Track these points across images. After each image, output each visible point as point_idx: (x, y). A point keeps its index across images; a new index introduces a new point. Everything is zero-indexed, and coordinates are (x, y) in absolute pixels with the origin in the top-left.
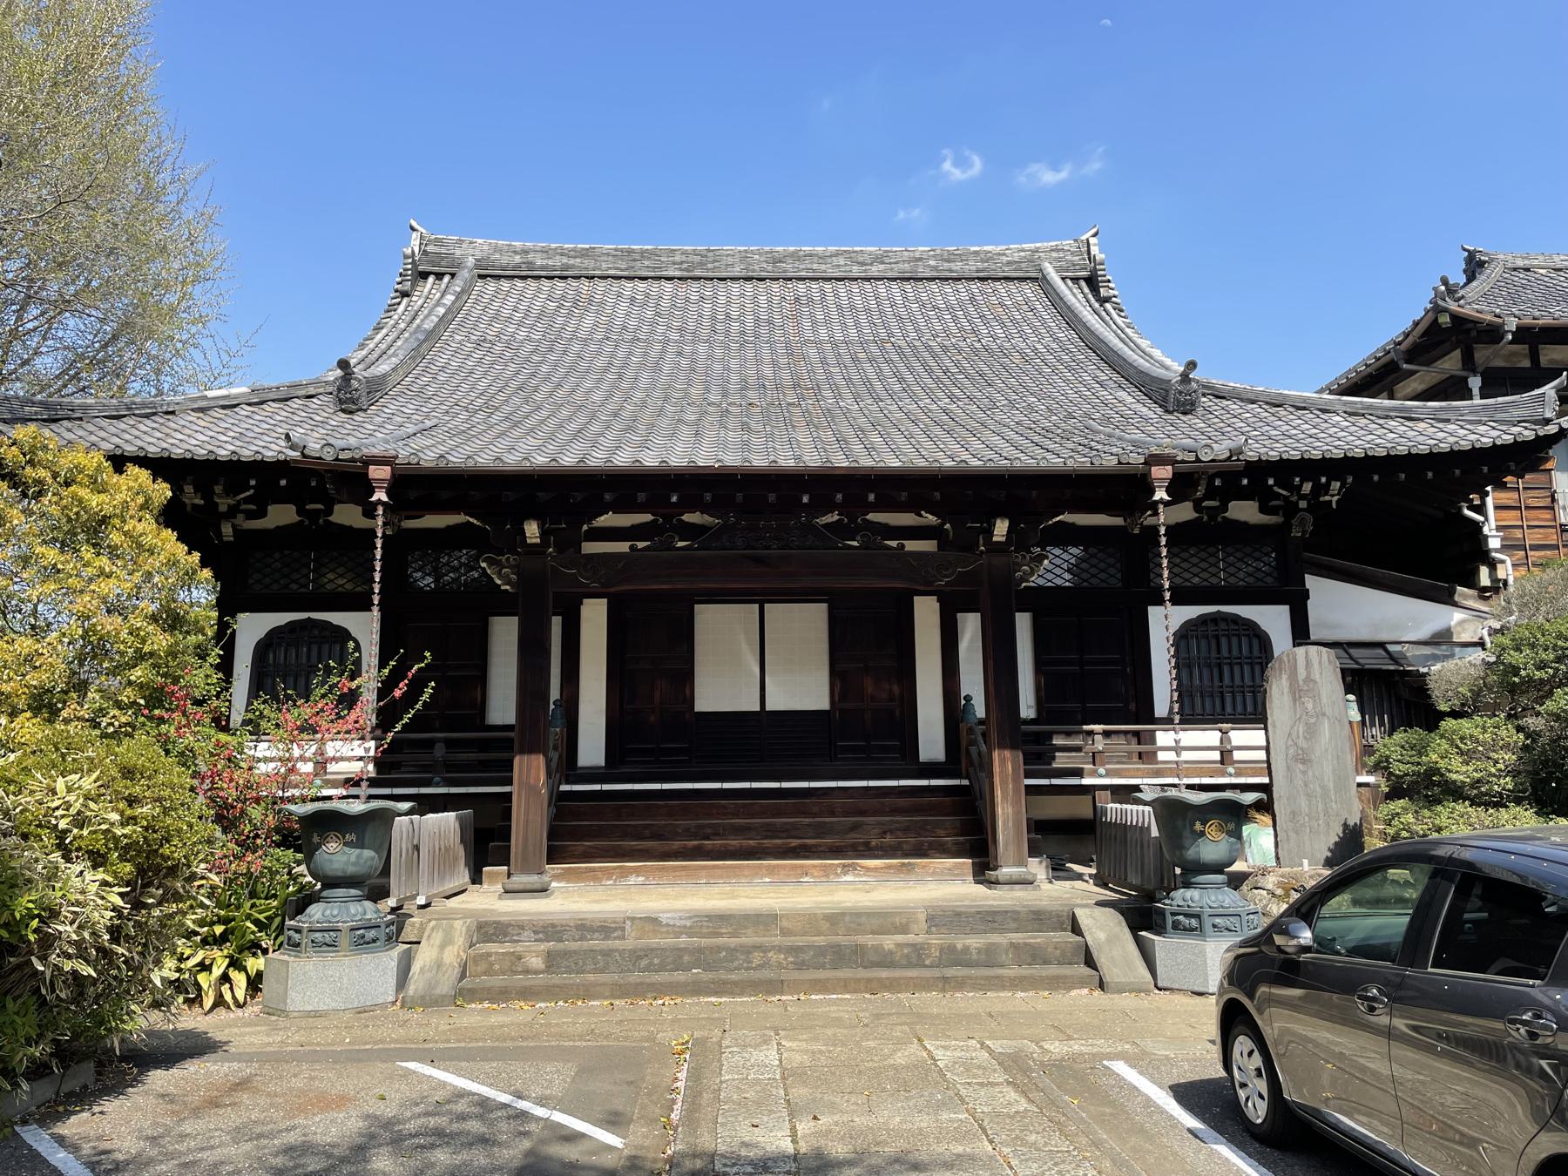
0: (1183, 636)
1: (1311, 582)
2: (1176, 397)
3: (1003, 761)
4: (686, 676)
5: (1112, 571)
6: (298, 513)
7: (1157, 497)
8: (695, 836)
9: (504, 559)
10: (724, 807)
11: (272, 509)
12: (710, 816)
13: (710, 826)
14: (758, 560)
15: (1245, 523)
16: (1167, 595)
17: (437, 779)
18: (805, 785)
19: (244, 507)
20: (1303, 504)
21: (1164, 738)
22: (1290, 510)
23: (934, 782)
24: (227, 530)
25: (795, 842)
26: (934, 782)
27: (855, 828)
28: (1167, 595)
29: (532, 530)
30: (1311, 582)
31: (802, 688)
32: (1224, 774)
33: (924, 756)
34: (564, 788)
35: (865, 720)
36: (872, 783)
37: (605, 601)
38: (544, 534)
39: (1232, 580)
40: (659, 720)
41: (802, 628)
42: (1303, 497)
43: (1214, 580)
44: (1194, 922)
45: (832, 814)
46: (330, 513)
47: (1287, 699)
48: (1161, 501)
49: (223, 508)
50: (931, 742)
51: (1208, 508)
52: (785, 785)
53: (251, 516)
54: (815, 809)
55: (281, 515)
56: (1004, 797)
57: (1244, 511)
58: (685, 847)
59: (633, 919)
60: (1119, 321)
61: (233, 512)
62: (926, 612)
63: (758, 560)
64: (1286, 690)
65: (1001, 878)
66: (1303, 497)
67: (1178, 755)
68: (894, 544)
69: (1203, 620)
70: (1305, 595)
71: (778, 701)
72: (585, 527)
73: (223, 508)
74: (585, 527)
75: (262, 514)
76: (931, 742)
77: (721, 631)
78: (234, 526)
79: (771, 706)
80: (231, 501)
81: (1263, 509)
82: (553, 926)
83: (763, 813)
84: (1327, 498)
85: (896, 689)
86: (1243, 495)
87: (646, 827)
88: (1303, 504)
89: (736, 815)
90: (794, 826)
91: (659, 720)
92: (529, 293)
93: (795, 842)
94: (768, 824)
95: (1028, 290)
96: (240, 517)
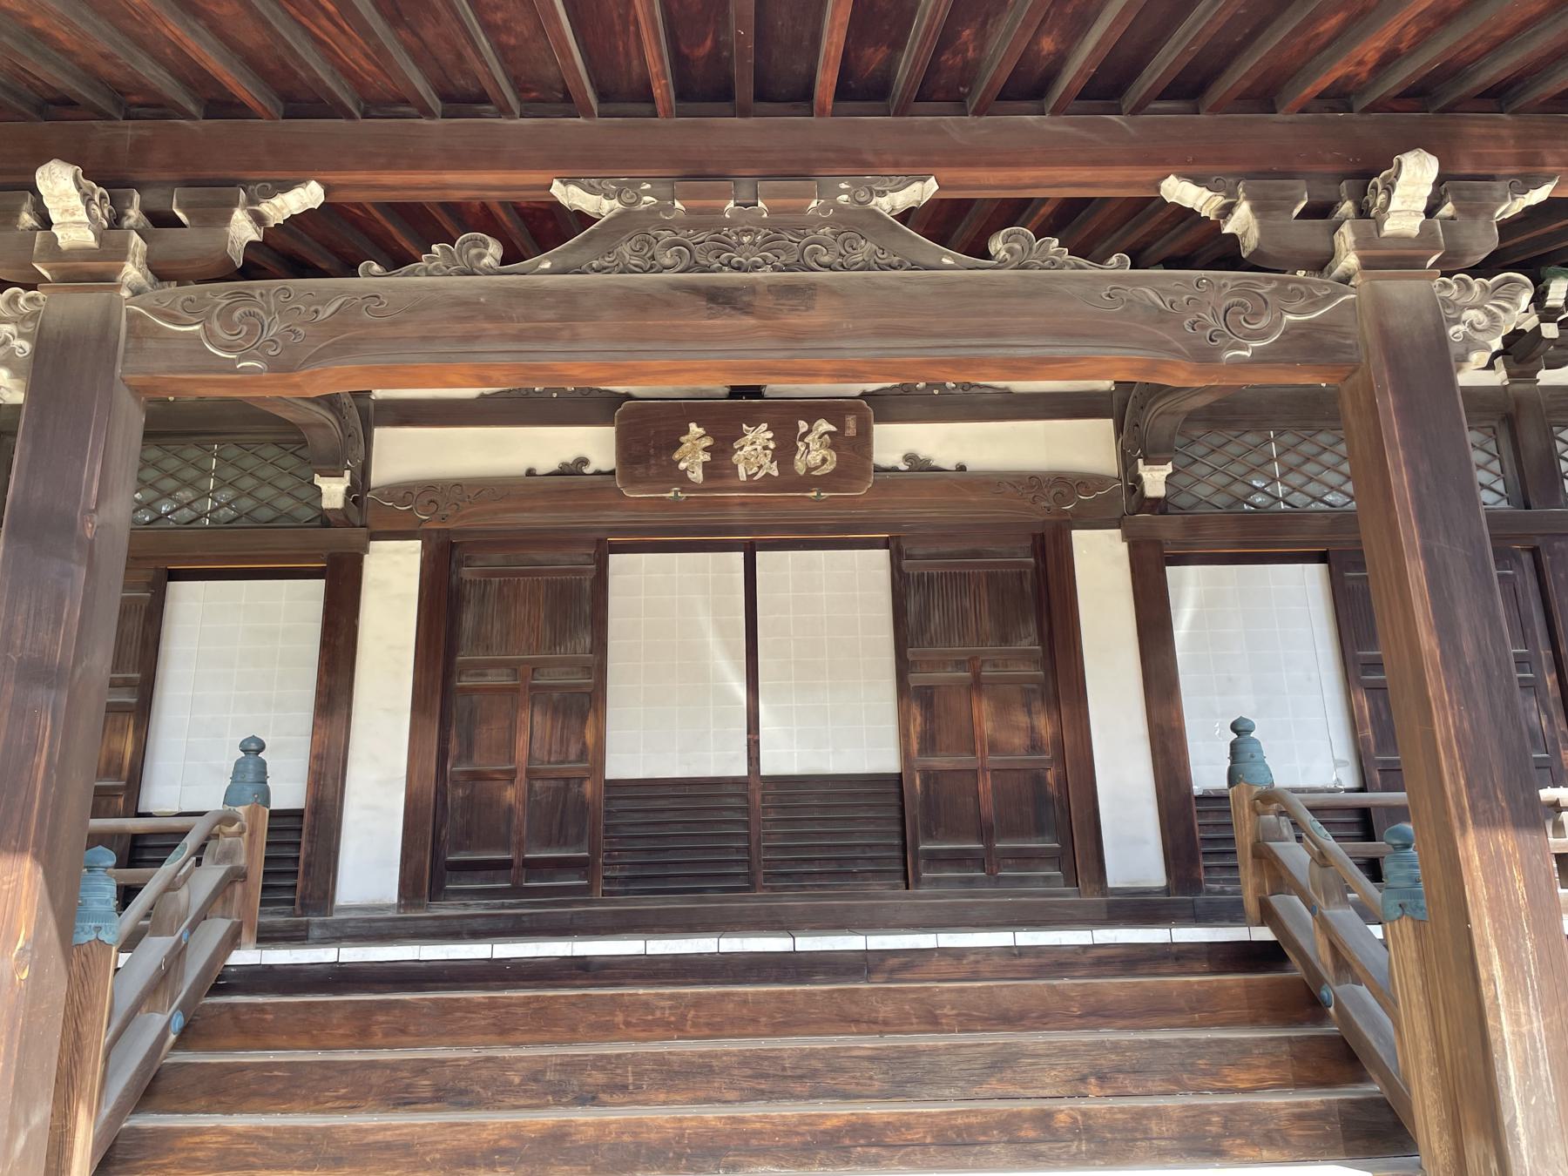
3: (1494, 867)
4: (585, 702)
8: (558, 1094)
10: (646, 1005)
12: (605, 1030)
13: (601, 1063)
14: (719, 298)
25: (838, 1112)
27: (1001, 1063)
31: (837, 720)
33: (1116, 877)
36: (1026, 938)
37: (417, 544)
41: (838, 598)
45: (932, 1022)
50: (1133, 849)
54: (886, 1010)
56: (1513, 965)
58: (517, 1133)
63: (719, 298)
76: (1133, 849)
77: (664, 604)
79: (766, 770)
83: (747, 1022)
85: (1045, 726)
87: (422, 1068)
89: (676, 1028)
90: (834, 1063)
93: (838, 1112)
94: (759, 1057)
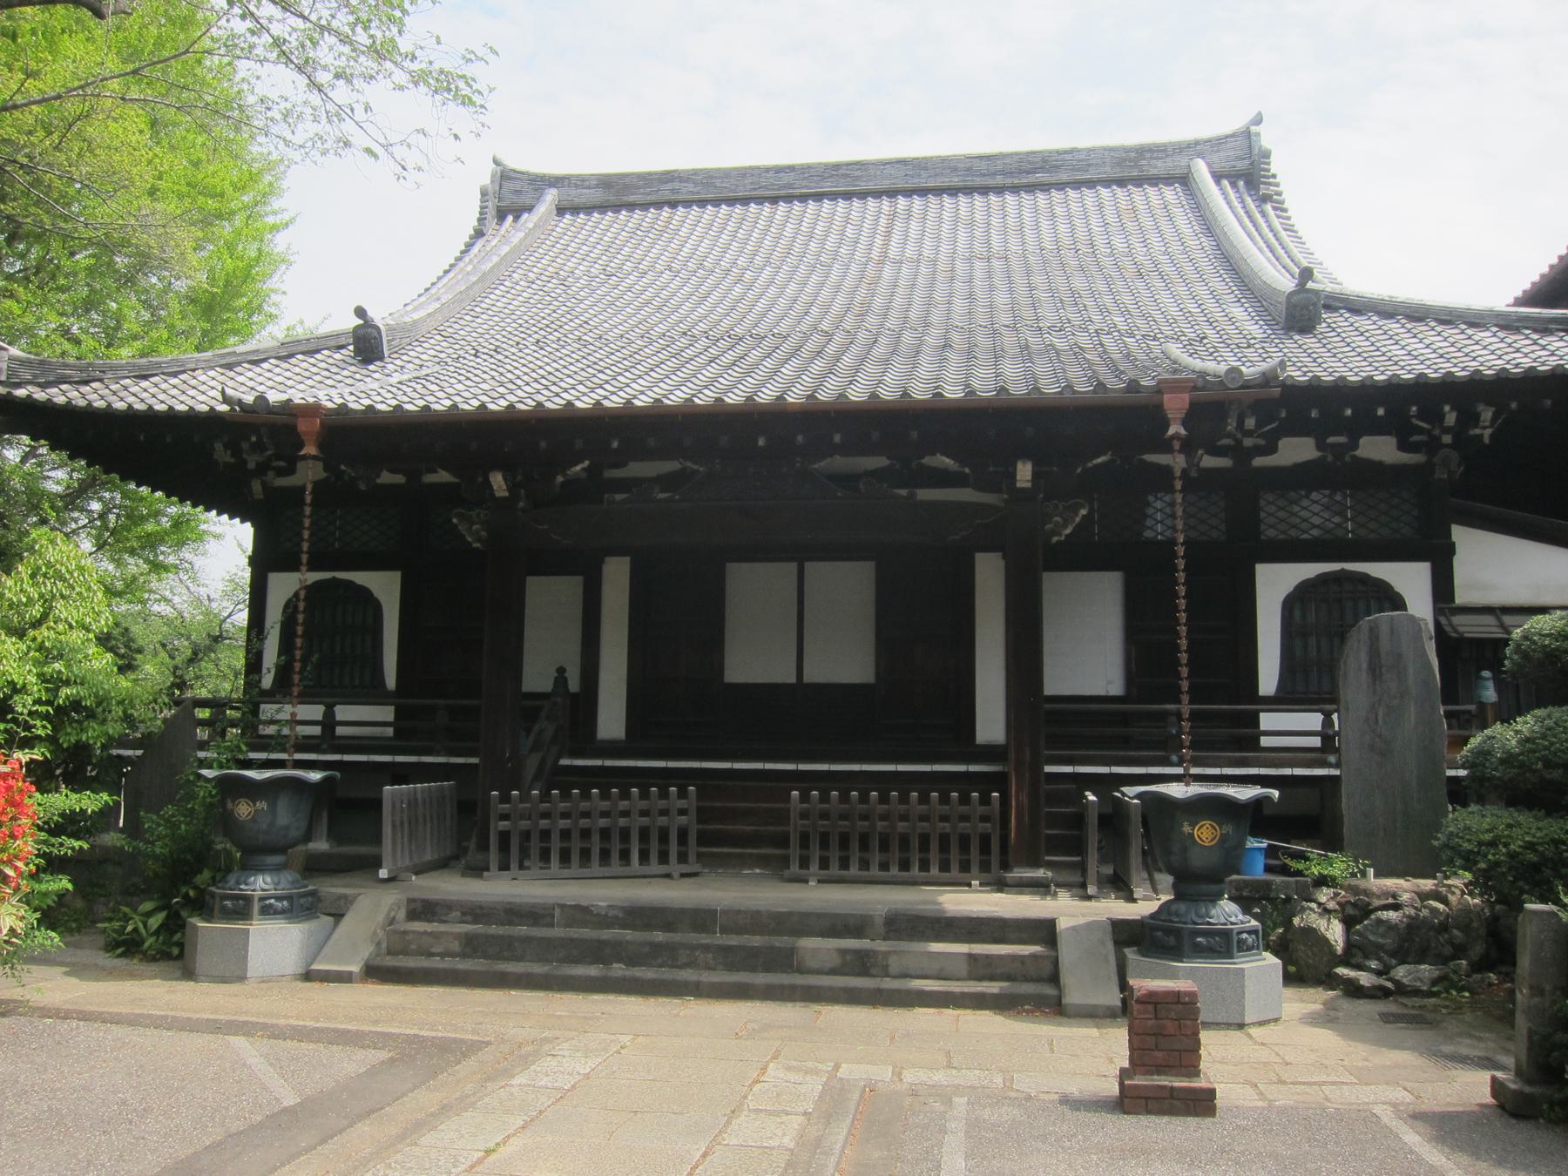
0: (1294, 603)
1: (1459, 534)
2: (1302, 312)
5: (1272, 520)
6: (325, 470)
7: (1171, 431)
9: (474, 514)
11: (1283, 443)
15: (1380, 464)
16: (305, 558)
17: (324, 746)
18: (824, 767)
19: (275, 464)
20: (1447, 439)
21: (1268, 721)
22: (1432, 446)
23: (973, 768)
24: (256, 486)
26: (973, 768)
28: (305, 558)
29: (498, 481)
30: (1459, 534)
31: (844, 658)
32: (1324, 764)
34: (564, 762)
35: (916, 695)
37: (627, 559)
38: (513, 487)
39: (1362, 532)
40: (685, 696)
42: (1447, 430)
43: (1340, 533)
44: (1172, 941)
46: (1356, 447)
47: (1364, 677)
48: (1176, 436)
49: (251, 465)
51: (1333, 445)
52: (803, 767)
53: (281, 473)
55: (1296, 451)
57: (1379, 449)
59: (562, 906)
60: (1276, 223)
61: (262, 469)
62: (989, 574)
64: (1364, 666)
65: (1009, 881)
66: (1447, 430)
67: (293, 714)
68: (904, 492)
69: (1323, 579)
70: (1450, 550)
71: (816, 673)
72: (560, 479)
73: (251, 465)
74: (560, 479)
75: (1271, 449)
76: (991, 724)
78: (264, 484)
80: (260, 459)
81: (1403, 446)
82: (481, 908)
84: (1477, 431)
86: (1378, 428)
88: (1447, 439)
91: (685, 696)
92: (750, 217)
95: (1170, 194)
96: (271, 474)
